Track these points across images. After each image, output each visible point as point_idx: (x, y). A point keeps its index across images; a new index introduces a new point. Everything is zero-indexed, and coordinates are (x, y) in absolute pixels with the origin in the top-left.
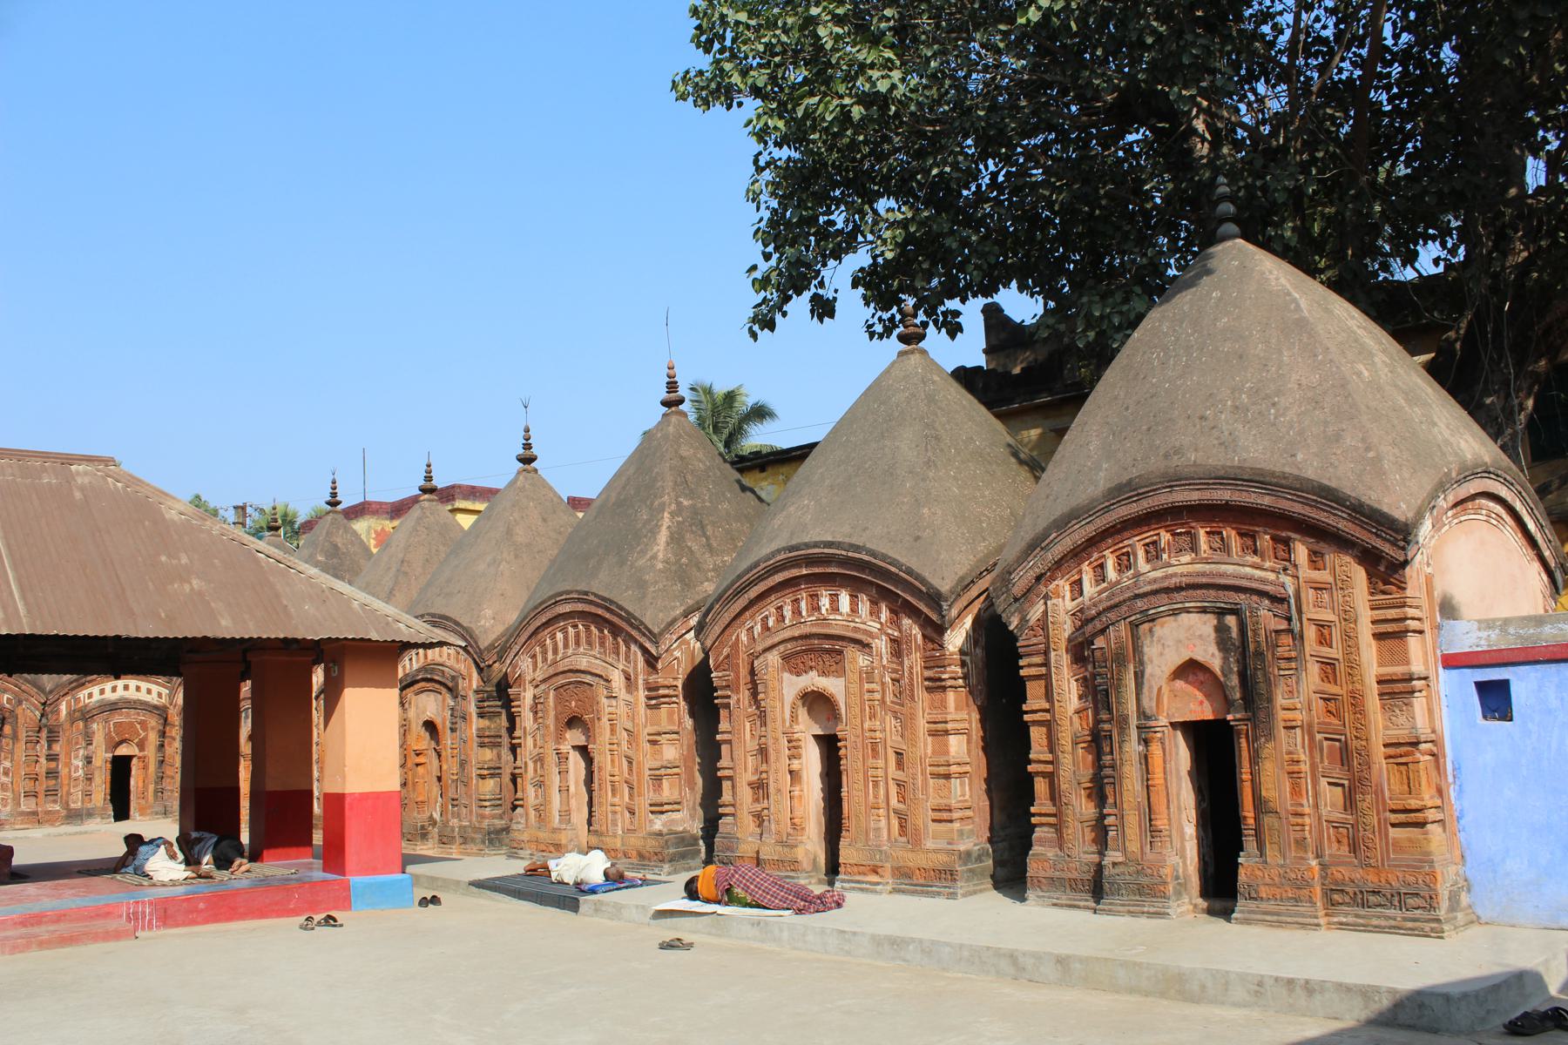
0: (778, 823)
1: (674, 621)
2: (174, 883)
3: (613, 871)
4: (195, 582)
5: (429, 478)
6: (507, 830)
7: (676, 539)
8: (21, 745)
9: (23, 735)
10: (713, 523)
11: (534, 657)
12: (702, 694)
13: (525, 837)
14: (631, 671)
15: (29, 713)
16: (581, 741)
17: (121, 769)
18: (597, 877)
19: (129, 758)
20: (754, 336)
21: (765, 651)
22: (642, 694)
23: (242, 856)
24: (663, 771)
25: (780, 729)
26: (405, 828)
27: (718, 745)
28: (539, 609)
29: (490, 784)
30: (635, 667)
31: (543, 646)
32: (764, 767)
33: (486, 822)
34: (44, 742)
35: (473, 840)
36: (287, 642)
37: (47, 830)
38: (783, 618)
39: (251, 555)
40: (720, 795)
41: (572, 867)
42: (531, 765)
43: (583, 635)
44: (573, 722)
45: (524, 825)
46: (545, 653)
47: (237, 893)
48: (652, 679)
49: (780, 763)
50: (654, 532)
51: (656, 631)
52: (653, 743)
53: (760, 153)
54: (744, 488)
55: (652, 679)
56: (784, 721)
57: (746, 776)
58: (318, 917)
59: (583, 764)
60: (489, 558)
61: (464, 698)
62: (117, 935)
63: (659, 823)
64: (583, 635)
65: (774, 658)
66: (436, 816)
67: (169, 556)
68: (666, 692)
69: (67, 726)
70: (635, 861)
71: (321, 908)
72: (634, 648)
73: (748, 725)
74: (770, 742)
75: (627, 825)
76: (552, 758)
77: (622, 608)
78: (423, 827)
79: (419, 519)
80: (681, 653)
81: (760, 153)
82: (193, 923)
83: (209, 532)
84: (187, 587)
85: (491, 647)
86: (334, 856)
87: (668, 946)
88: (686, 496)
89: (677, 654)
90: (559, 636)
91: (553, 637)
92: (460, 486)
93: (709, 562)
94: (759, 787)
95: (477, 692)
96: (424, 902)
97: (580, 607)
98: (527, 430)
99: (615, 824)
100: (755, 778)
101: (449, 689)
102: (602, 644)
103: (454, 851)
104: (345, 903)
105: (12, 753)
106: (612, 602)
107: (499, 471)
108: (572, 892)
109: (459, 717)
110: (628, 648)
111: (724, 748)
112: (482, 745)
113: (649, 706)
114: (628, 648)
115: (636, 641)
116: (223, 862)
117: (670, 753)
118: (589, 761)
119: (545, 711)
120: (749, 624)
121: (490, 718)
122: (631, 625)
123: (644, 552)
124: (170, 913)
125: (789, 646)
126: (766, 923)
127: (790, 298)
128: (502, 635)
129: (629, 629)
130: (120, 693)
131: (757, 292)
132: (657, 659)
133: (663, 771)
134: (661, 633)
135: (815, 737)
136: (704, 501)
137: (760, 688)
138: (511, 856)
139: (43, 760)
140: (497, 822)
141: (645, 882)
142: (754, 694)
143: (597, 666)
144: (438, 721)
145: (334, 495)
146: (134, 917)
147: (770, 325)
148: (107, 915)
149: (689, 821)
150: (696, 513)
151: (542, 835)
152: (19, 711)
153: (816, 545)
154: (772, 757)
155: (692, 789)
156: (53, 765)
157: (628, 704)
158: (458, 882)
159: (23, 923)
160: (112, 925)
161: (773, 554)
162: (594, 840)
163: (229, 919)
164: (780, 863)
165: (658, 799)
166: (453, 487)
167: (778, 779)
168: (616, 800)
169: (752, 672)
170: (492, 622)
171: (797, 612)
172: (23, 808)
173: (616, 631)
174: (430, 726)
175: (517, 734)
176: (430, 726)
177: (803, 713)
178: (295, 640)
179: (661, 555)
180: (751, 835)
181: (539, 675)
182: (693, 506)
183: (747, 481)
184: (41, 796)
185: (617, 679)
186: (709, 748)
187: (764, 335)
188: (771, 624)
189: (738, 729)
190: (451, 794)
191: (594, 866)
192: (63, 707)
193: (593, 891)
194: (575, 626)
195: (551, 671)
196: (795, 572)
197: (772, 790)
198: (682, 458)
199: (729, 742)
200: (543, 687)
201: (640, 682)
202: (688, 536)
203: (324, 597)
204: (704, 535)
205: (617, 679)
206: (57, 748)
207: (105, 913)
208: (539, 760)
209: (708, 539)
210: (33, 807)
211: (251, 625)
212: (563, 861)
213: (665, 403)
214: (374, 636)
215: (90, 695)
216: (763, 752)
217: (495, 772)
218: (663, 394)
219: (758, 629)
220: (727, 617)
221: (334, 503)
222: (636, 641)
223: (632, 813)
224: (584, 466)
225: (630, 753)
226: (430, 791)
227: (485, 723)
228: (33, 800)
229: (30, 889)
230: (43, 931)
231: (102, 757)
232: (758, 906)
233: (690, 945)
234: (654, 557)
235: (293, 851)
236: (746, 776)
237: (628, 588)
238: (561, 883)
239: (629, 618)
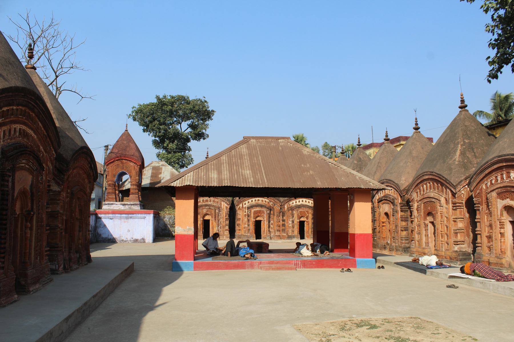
0: (496, 250)
1: (462, 181)
2: (308, 256)
3: (439, 262)
4: (311, 172)
5: (387, 136)
6: (409, 247)
7: (463, 154)
9: (276, 214)
10: (477, 148)
11: (417, 193)
12: (471, 206)
13: (415, 250)
14: (447, 198)
15: (277, 208)
16: (432, 220)
17: (302, 224)
18: (434, 264)
19: (304, 221)
20: (489, 81)
21: (491, 191)
22: (451, 205)
23: (327, 250)
24: (458, 231)
25: (496, 218)
26: (376, 245)
27: (476, 223)
28: (418, 177)
29: (404, 233)
30: (449, 196)
31: (420, 189)
32: (491, 231)
33: (403, 245)
34: (281, 216)
35: (399, 250)
36: (337, 189)
37: (283, 241)
38: (498, 180)
39: (327, 164)
40: (477, 240)
41: (424, 260)
42: (416, 227)
43: (432, 186)
44: (429, 214)
45: (414, 246)
46: (420, 191)
47: (324, 260)
48: (454, 200)
49: (497, 229)
50: (455, 152)
51: (455, 184)
52: (455, 221)
53: (494, 14)
54: (489, 135)
55: (454, 200)
56: (498, 215)
57: (485, 234)
58: (345, 269)
59: (433, 228)
60: (404, 161)
61: (396, 205)
62: (291, 269)
63: (456, 248)
64: (432, 186)
65: (494, 194)
66: (389, 242)
67: (304, 165)
68: (459, 205)
69: (287, 212)
70: (449, 260)
71: (347, 266)
72: (448, 190)
73: (486, 217)
74: (493, 222)
75: (446, 248)
76: (423, 226)
77: (444, 177)
78: (384, 245)
79: (384, 149)
80: (464, 193)
81: (494, 14)
82: (312, 267)
83: (315, 157)
84: (309, 173)
85: (404, 189)
86: (352, 253)
87: (449, 287)
88: (467, 139)
89: (463, 192)
90: (425, 186)
91: (423, 186)
92: (402, 137)
93: (475, 161)
94: (489, 237)
95: (400, 204)
96: (379, 267)
97: (431, 177)
98: (416, 119)
99: (442, 247)
100: (488, 235)
101: (392, 203)
102: (438, 189)
103: (393, 253)
104: (355, 266)
105: (273, 219)
106: (440, 175)
107: (409, 132)
108: (424, 268)
109: (395, 211)
110: (446, 190)
111: (478, 224)
112: (402, 221)
113: (453, 209)
114: (446, 190)
115: (449, 188)
116: (322, 252)
117: (460, 225)
118: (434, 226)
119: (421, 210)
120: (486, 182)
121: (404, 212)
122: (447, 183)
123: (451, 158)
124: (306, 264)
125: (499, 190)
126: (485, 283)
127: (503, 66)
128: (408, 186)
129: (446, 184)
130: (301, 202)
131: (491, 66)
132: (455, 194)
133: (458, 231)
134: (457, 185)
135: (510, 221)
136: (473, 140)
137: (490, 204)
138: (410, 256)
139: (281, 221)
140: (406, 245)
141: (450, 267)
142: (488, 206)
143: (436, 196)
144: (389, 213)
145: (359, 142)
146: (296, 264)
147: (496, 77)
148: (289, 263)
149: (467, 248)
150: (471, 145)
151: (420, 250)
152: (275, 207)
153: (508, 155)
154: (494, 228)
155: (468, 237)
156: (284, 223)
157: (446, 208)
158: (391, 263)
159: (269, 263)
160: (290, 266)
161: (493, 158)
162: (436, 252)
163: (322, 267)
164: (496, 264)
165: (456, 240)
166: (400, 137)
167: (496, 235)
168: (443, 240)
169: (487, 199)
170: (404, 181)
171: (502, 178)
173: (442, 184)
174: (386, 214)
175: (413, 217)
176: (386, 214)
177: (505, 213)
178: (339, 188)
179: (457, 159)
180: (487, 254)
181: (419, 199)
182: (469, 142)
183: (490, 132)
184: (281, 231)
185: (443, 200)
186: (474, 224)
187: (494, 81)
188: (493, 182)
189: (482, 217)
190: (393, 235)
191: (433, 260)
192: (286, 206)
193: (431, 268)
194: (429, 183)
195: (422, 198)
196: (501, 165)
197: (494, 239)
198: (466, 126)
199: (479, 222)
200: (420, 202)
201: (450, 201)
202: (467, 152)
203: (348, 175)
204: (473, 152)
205: (443, 200)
206: (285, 218)
207: (288, 263)
208: (419, 226)
209: (475, 153)
210: (279, 234)
211: (326, 184)
212: (423, 258)
213: (460, 107)
214: (362, 187)
215: (293, 203)
216: (491, 226)
217: (406, 229)
218: (459, 104)
219: (489, 184)
220: (478, 180)
221: (359, 145)
222: (449, 188)
223: (448, 244)
224: (435, 129)
225: (447, 224)
226: (387, 234)
227: (403, 213)
229: (272, 255)
230: (273, 266)
231: (297, 221)
232: (484, 277)
233: (457, 287)
234: (455, 160)
235: (342, 250)
236: (485, 234)
237: (446, 171)
238: (423, 265)
239: (446, 180)
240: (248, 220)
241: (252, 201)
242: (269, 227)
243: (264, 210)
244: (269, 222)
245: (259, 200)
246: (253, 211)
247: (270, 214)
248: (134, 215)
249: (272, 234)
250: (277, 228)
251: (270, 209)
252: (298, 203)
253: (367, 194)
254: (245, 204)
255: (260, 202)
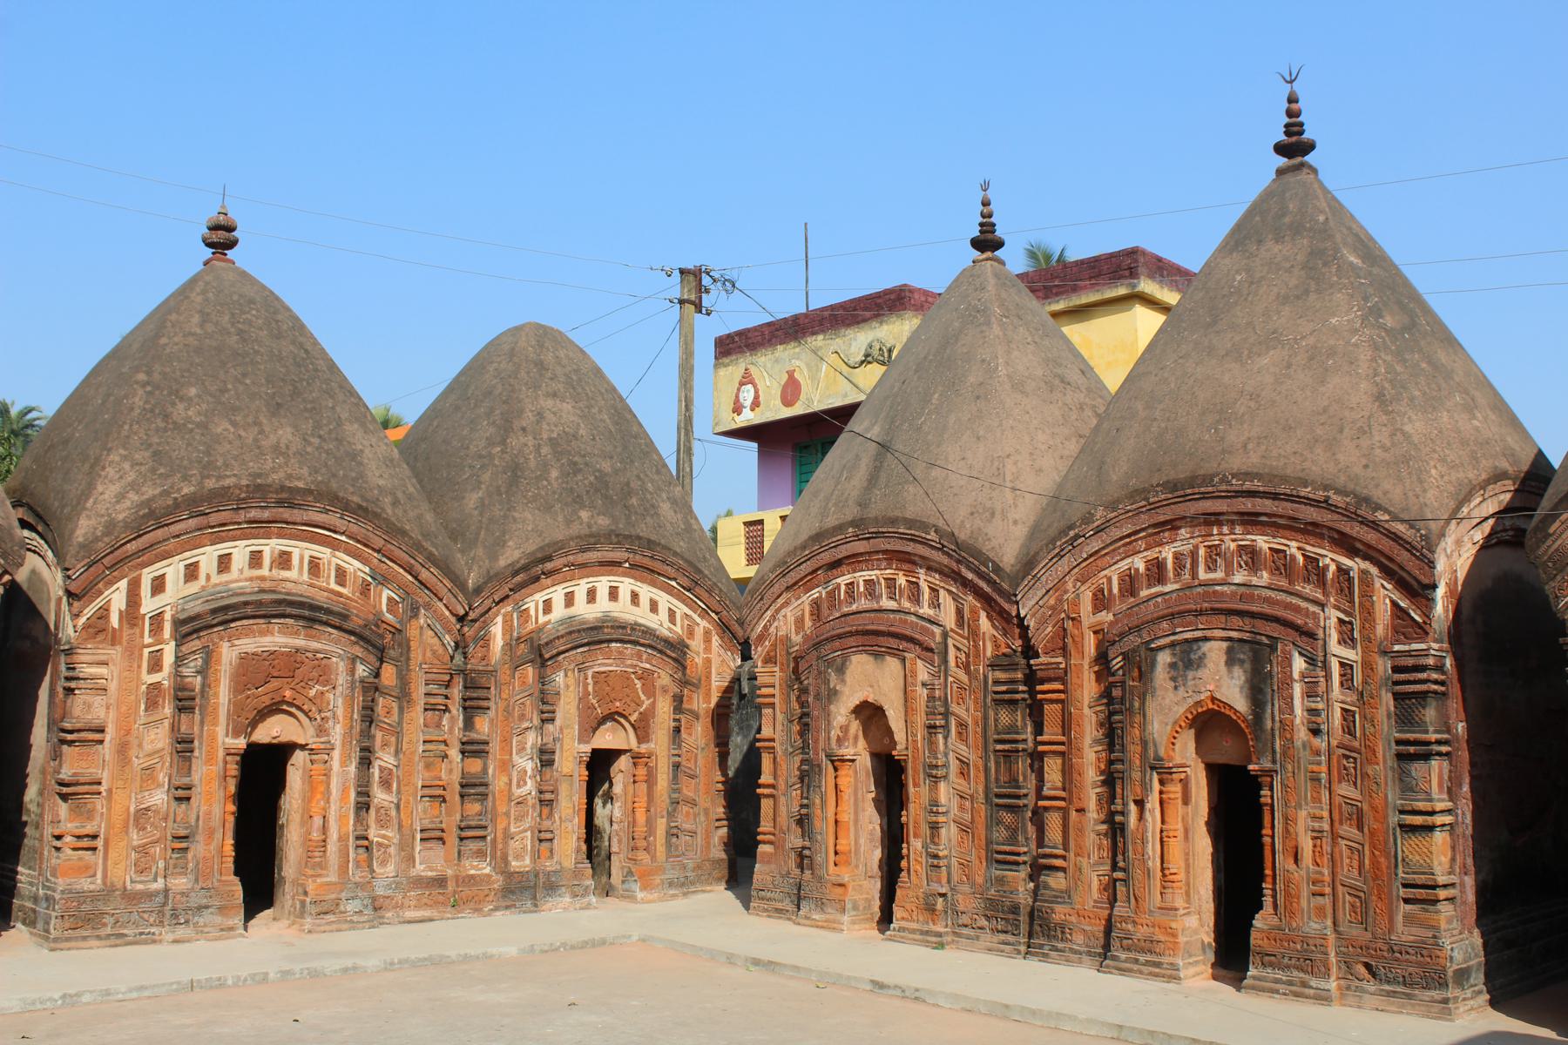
8: (417, 716)
9: (419, 690)
34: (456, 711)
92: (1144, 253)
105: (397, 732)
130: (603, 605)
139: (454, 753)
152: (412, 631)
156: (475, 765)
172: (420, 869)
192: (497, 629)
206: (483, 725)
228: (437, 851)
240: (184, 747)
241: (224, 562)
242: (363, 806)
243: (330, 646)
244: (366, 762)
245: (284, 560)
246: (229, 652)
247: (372, 688)
248: (73, 944)
249: (387, 871)
250: (421, 813)
251: (377, 642)
252: (584, 610)
253: (303, 747)
254: (159, 586)
255: (296, 578)
